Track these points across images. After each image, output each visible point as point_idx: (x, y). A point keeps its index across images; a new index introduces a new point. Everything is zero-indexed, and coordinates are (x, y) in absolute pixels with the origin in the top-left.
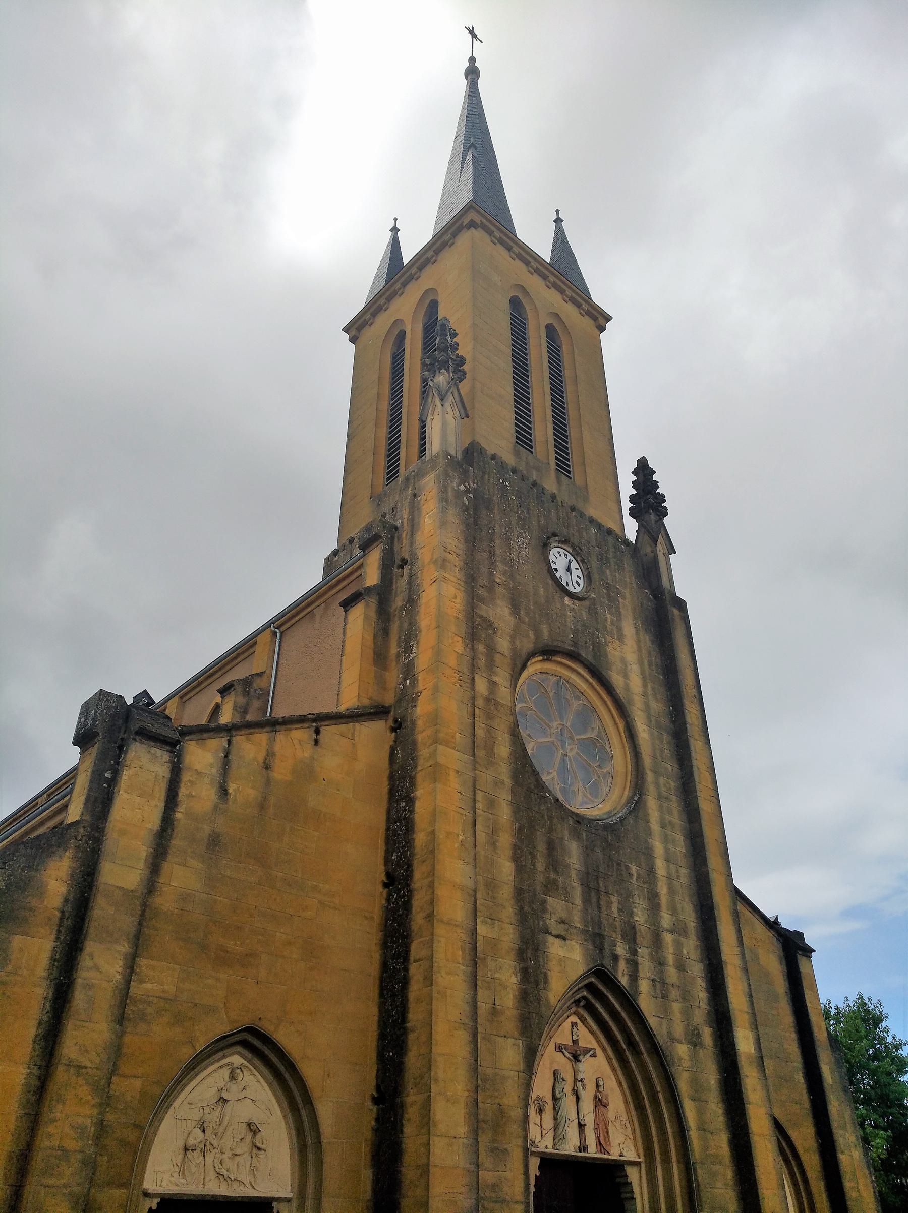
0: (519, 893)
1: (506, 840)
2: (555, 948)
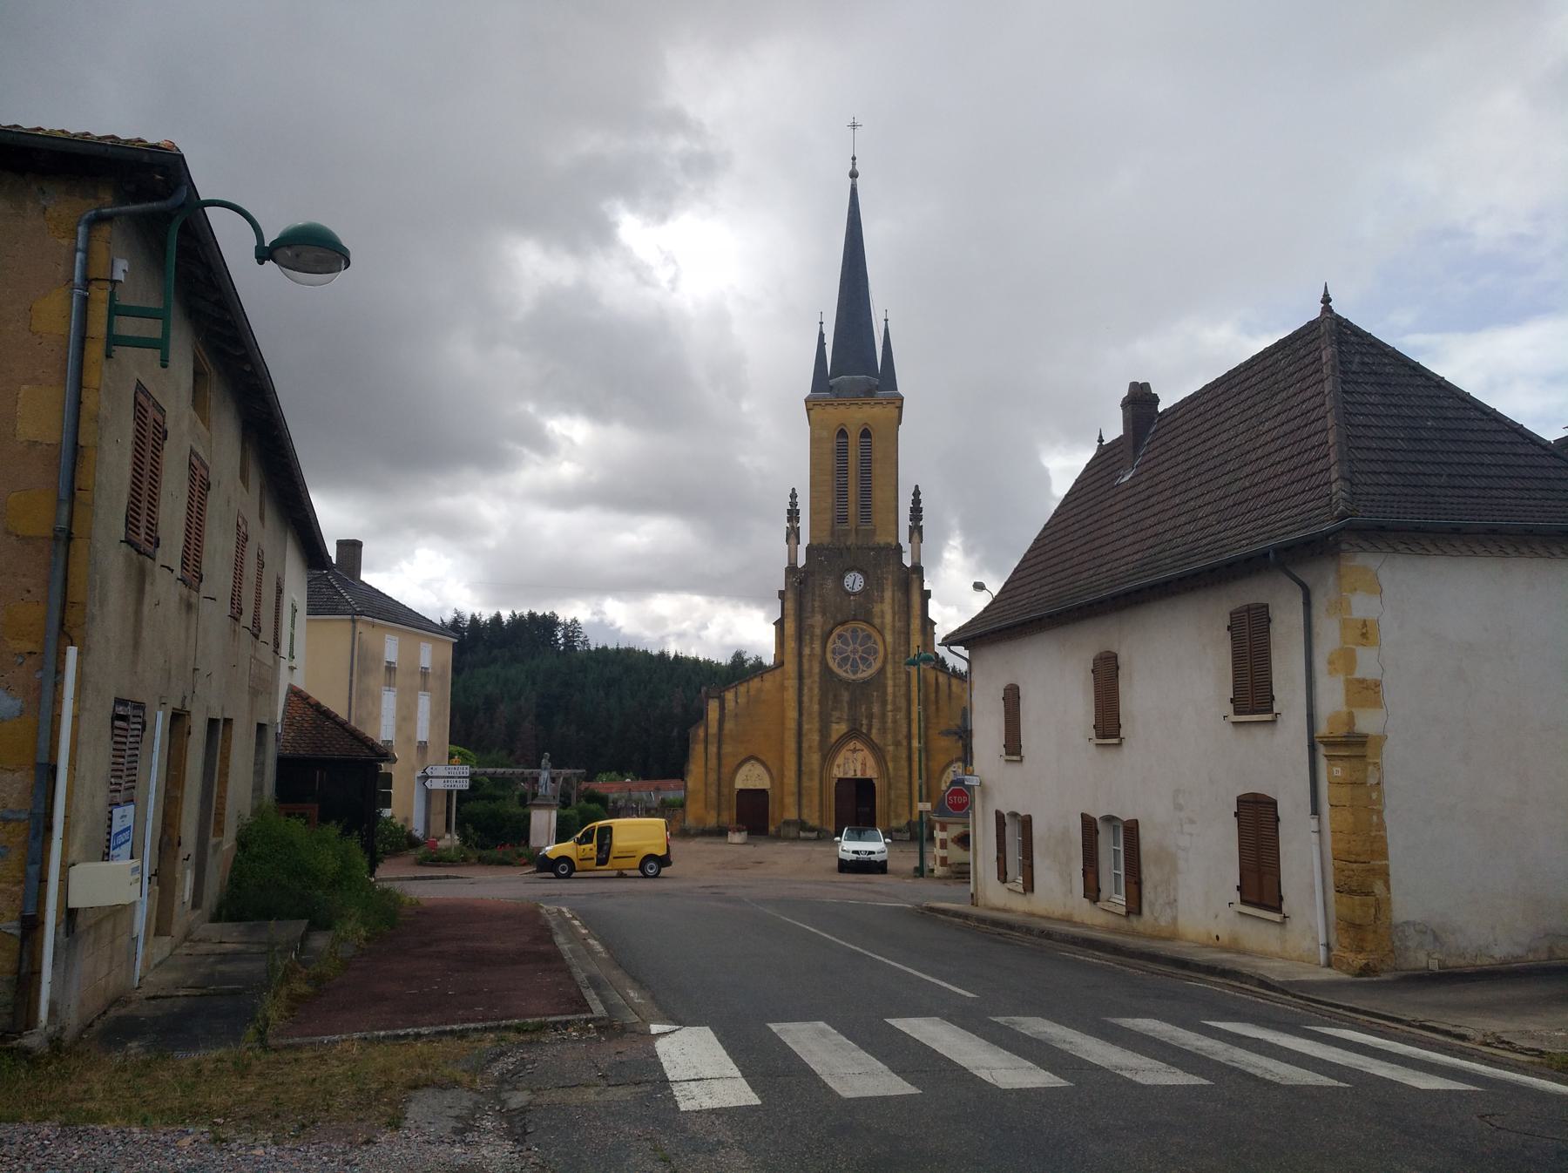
0: (821, 713)
1: (816, 699)
2: (835, 726)
